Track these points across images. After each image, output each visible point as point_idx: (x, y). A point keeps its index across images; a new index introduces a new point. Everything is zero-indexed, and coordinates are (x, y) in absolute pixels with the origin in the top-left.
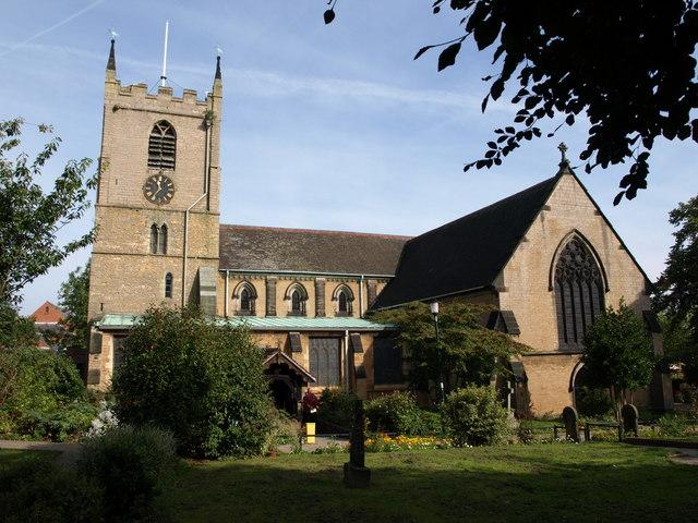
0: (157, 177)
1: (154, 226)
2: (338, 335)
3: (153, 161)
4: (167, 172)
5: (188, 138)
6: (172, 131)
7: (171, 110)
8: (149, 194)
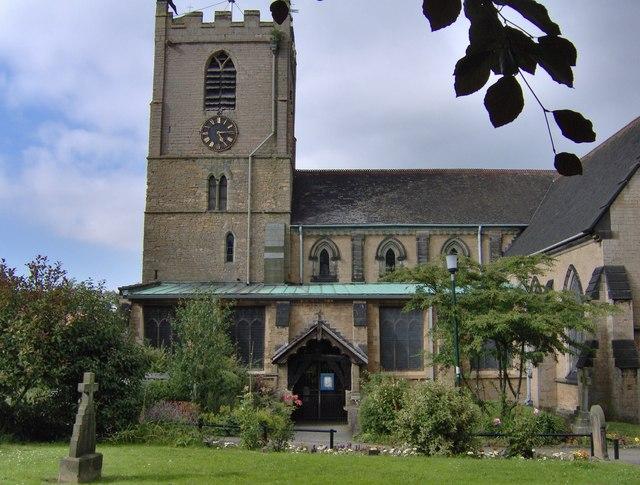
0: (215, 119)
1: (211, 178)
2: (388, 305)
3: (230, 84)
4: (226, 112)
5: (251, 69)
6: (230, 64)
7: (230, 38)
8: (207, 139)
